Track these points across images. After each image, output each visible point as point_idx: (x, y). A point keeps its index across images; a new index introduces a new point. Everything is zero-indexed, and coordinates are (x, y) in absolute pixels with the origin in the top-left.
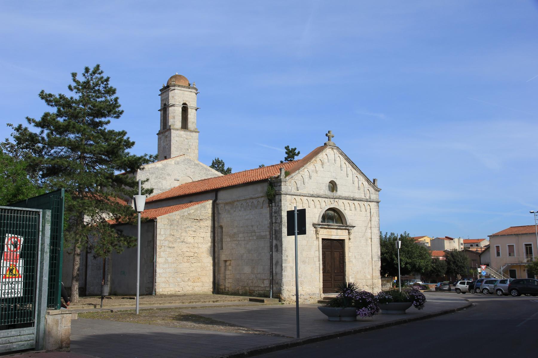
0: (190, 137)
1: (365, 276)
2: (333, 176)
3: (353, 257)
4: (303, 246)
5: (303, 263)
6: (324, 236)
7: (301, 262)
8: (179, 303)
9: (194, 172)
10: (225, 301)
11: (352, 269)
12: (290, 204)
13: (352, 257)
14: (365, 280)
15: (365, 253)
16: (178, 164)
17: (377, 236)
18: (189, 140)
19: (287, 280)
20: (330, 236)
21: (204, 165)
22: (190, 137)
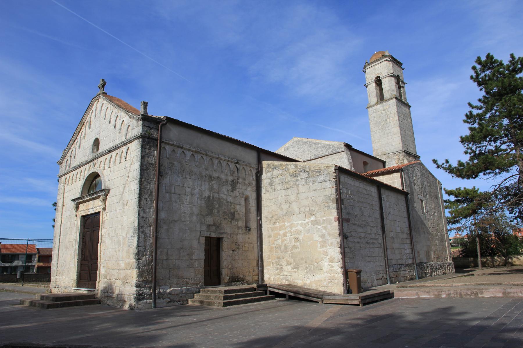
1: (118, 264)
3: (107, 236)
9: (303, 151)
16: (287, 149)
17: (135, 194)
18: (386, 111)
20: (87, 211)
21: (313, 140)
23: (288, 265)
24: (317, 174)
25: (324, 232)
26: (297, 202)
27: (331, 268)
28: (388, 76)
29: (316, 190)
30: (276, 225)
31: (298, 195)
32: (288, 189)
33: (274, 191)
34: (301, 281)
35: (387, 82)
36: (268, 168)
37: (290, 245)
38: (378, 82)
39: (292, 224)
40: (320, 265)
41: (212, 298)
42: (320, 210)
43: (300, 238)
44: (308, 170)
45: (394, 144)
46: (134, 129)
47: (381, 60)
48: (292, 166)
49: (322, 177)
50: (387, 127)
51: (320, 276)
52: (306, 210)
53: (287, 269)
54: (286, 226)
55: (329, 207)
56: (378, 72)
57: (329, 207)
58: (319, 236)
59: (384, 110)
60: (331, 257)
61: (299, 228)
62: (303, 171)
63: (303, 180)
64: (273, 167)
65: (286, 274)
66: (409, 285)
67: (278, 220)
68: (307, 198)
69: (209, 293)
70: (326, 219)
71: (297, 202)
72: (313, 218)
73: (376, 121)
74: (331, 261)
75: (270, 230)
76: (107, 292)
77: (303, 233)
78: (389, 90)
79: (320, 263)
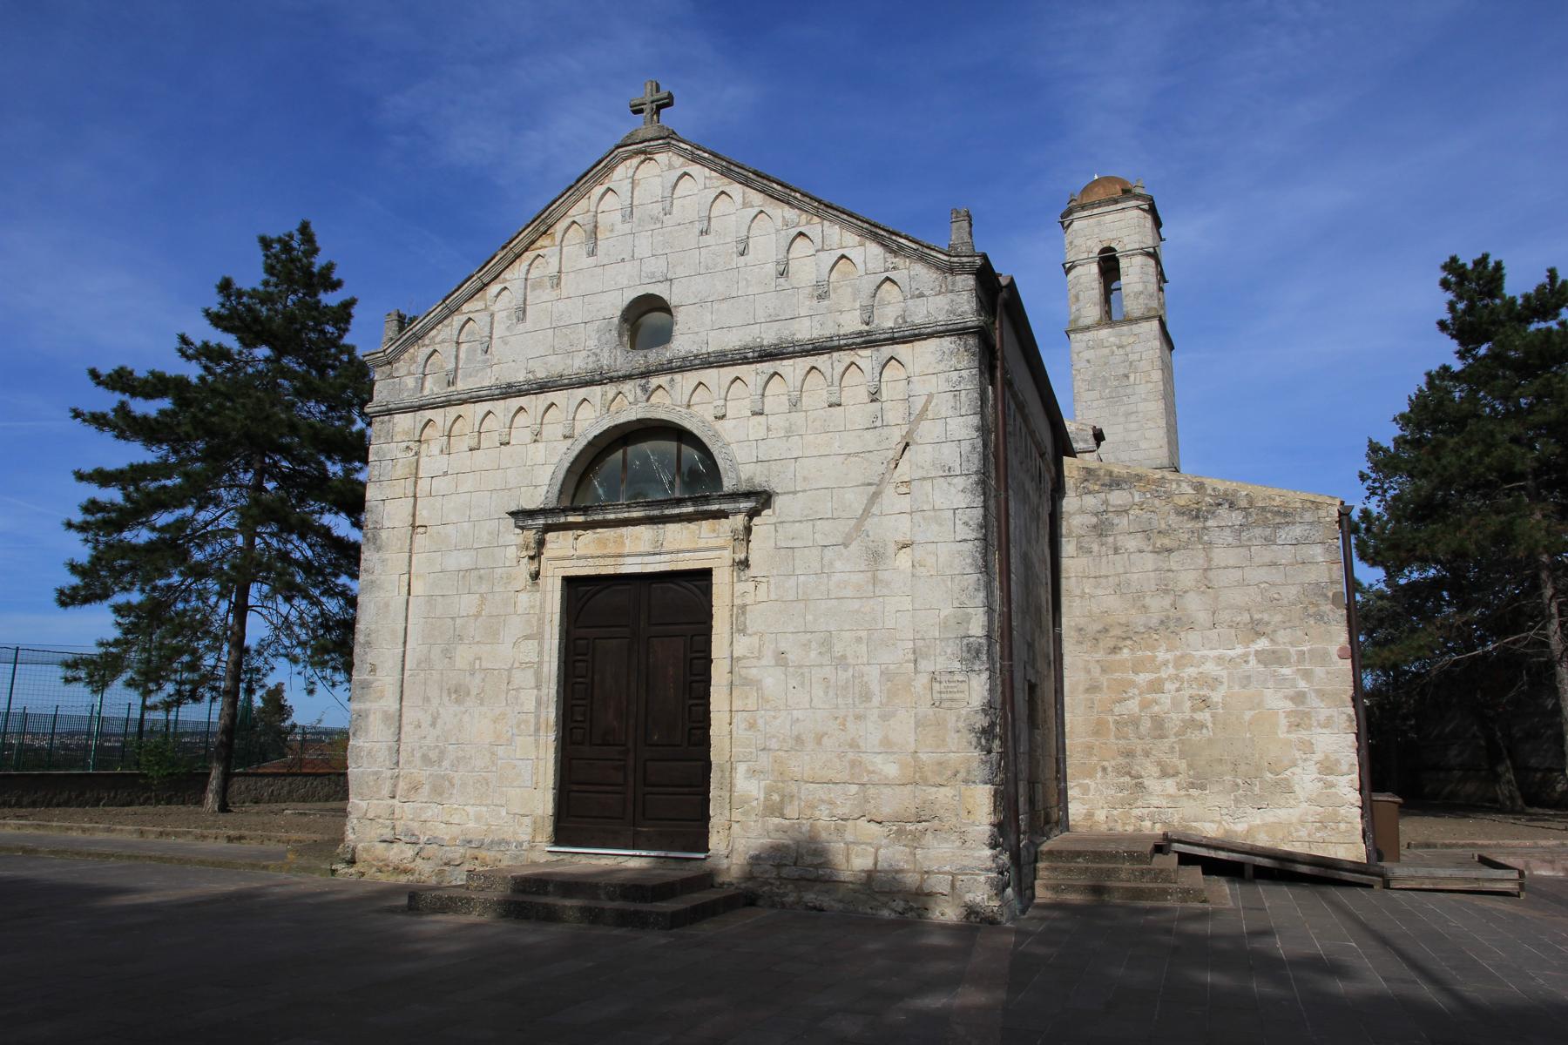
0: (1131, 340)
2: (653, 275)
3: (768, 659)
4: (458, 621)
5: (454, 696)
6: (574, 562)
7: (445, 694)
8: (130, 833)
10: (266, 842)
11: (752, 726)
12: (408, 447)
13: (758, 658)
14: (854, 789)
15: (864, 634)
18: (1128, 349)
19: (363, 773)
20: (611, 561)
22: (1131, 340)
23: (1164, 774)
24: (1278, 520)
25: (1302, 685)
26: (1203, 592)
27: (1326, 788)
28: (1141, 254)
29: (1274, 564)
30: (1118, 657)
31: (1209, 572)
32: (1170, 551)
33: (1111, 552)
34: (1214, 826)
35: (1138, 269)
36: (1086, 480)
37: (1175, 720)
38: (1109, 265)
39: (1182, 657)
40: (1286, 779)
41: (1123, 876)
42: (1288, 624)
43: (1215, 700)
44: (1244, 504)
45: (1143, 445)
46: (921, 295)
47: (1124, 202)
48: (1184, 485)
49: (1298, 531)
50: (1128, 396)
51: (1283, 810)
52: (1239, 619)
53: (1159, 788)
54: (1159, 659)
55: (1320, 617)
56: (1110, 235)
57: (1322, 617)
58: (1286, 697)
59: (1119, 347)
60: (1327, 757)
61: (1210, 668)
62: (1227, 506)
63: (1228, 530)
64: (1107, 480)
65: (1155, 802)
66: (1441, 841)
67: (1129, 642)
68: (1243, 583)
69: (1080, 860)
70: (1310, 651)
71: (1203, 592)
72: (1263, 644)
73: (1094, 374)
74: (1328, 768)
75: (1096, 671)
76: (795, 864)
77: (1225, 686)
78: (1141, 293)
79: (1288, 773)
